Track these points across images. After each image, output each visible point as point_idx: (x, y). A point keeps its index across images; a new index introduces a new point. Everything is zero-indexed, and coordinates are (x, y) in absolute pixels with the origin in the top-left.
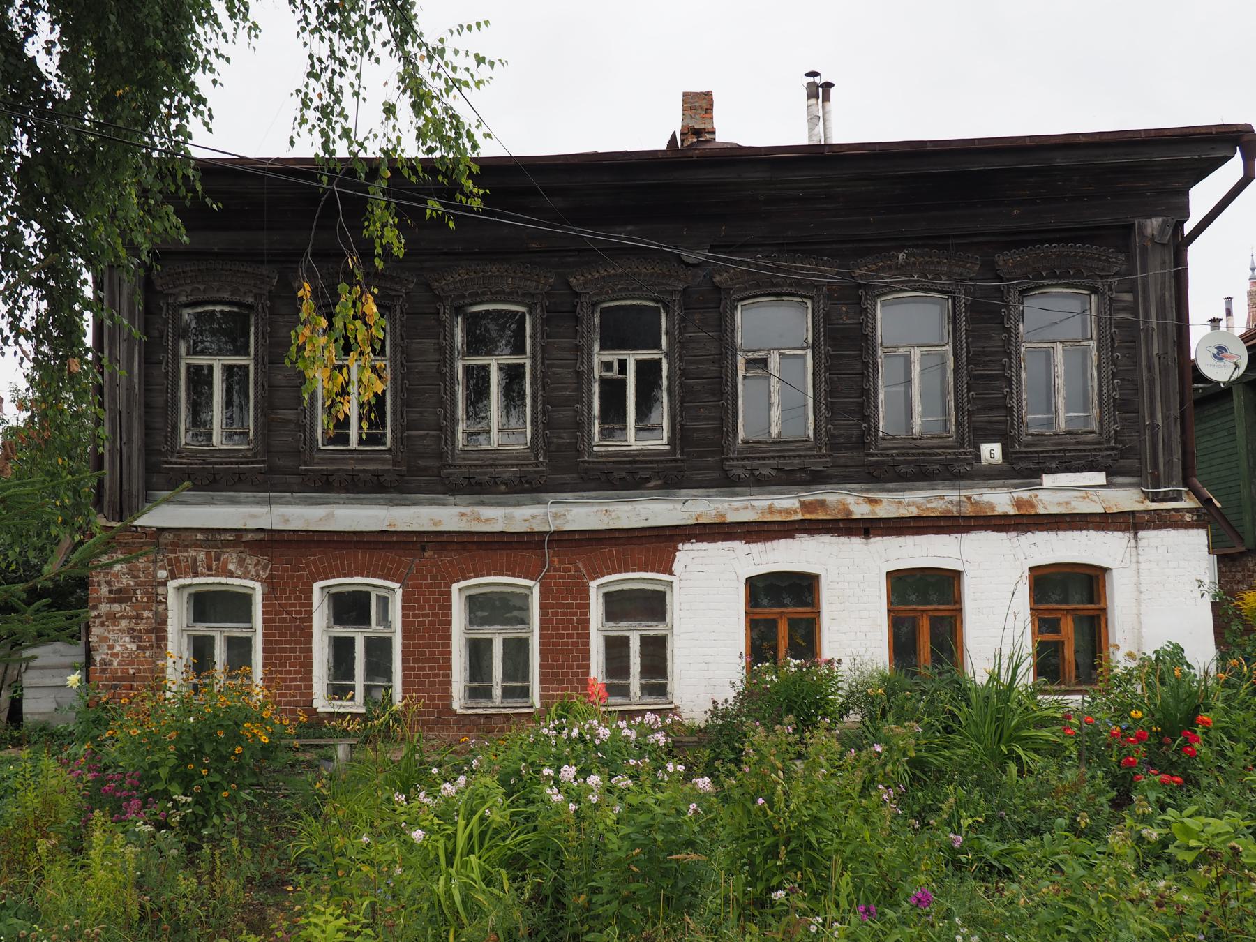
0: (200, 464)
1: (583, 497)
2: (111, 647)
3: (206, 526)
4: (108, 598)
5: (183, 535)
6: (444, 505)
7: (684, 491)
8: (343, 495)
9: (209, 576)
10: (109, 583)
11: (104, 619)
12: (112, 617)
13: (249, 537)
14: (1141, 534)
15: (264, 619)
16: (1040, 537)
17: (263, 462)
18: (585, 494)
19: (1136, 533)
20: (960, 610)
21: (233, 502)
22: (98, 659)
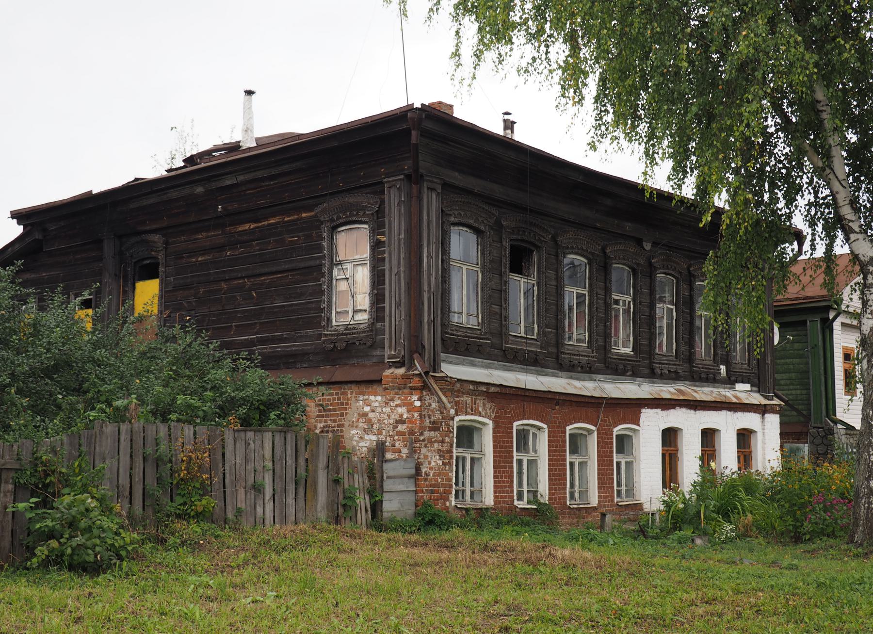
0: (463, 336)
1: (606, 378)
2: (430, 463)
3: (474, 379)
4: (429, 427)
5: (465, 385)
6: (557, 377)
7: (638, 379)
8: (519, 366)
9: (472, 414)
10: (429, 416)
11: (426, 442)
12: (431, 441)
13: (492, 389)
14: (767, 415)
15: (548, 440)
16: (739, 414)
17: (488, 339)
18: (608, 376)
19: (763, 415)
20: (715, 451)
21: (473, 365)
22: (423, 471)
